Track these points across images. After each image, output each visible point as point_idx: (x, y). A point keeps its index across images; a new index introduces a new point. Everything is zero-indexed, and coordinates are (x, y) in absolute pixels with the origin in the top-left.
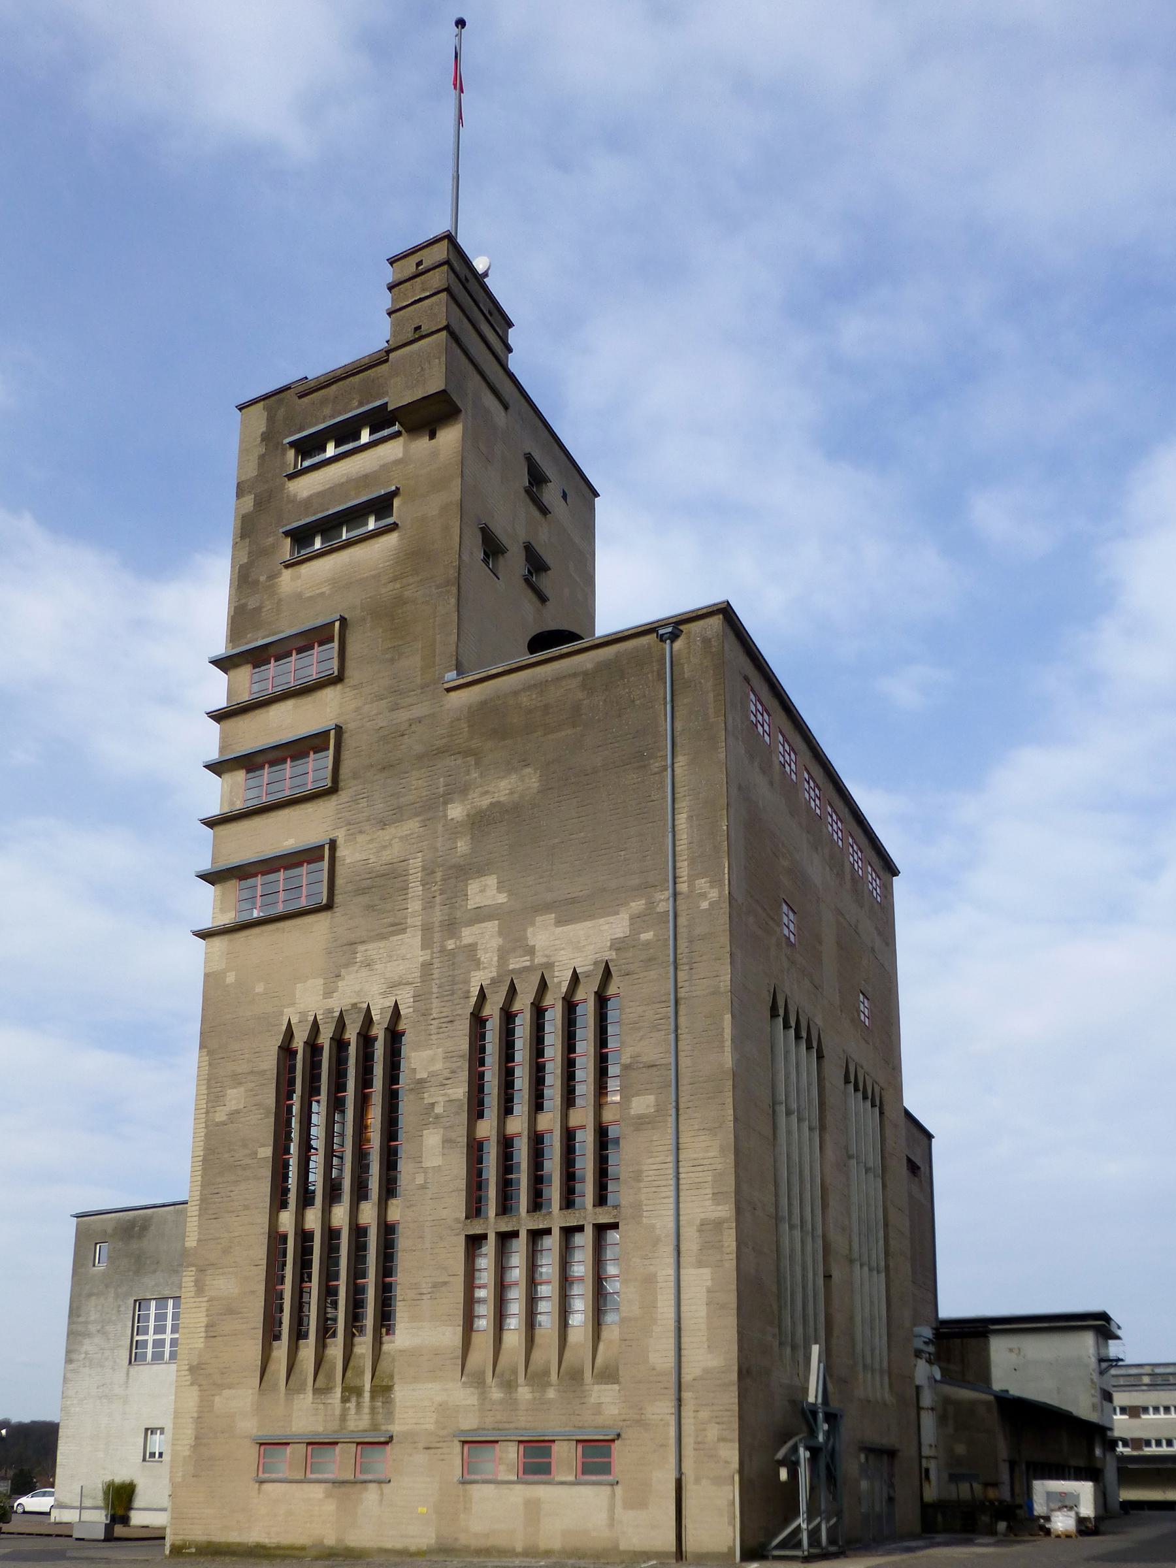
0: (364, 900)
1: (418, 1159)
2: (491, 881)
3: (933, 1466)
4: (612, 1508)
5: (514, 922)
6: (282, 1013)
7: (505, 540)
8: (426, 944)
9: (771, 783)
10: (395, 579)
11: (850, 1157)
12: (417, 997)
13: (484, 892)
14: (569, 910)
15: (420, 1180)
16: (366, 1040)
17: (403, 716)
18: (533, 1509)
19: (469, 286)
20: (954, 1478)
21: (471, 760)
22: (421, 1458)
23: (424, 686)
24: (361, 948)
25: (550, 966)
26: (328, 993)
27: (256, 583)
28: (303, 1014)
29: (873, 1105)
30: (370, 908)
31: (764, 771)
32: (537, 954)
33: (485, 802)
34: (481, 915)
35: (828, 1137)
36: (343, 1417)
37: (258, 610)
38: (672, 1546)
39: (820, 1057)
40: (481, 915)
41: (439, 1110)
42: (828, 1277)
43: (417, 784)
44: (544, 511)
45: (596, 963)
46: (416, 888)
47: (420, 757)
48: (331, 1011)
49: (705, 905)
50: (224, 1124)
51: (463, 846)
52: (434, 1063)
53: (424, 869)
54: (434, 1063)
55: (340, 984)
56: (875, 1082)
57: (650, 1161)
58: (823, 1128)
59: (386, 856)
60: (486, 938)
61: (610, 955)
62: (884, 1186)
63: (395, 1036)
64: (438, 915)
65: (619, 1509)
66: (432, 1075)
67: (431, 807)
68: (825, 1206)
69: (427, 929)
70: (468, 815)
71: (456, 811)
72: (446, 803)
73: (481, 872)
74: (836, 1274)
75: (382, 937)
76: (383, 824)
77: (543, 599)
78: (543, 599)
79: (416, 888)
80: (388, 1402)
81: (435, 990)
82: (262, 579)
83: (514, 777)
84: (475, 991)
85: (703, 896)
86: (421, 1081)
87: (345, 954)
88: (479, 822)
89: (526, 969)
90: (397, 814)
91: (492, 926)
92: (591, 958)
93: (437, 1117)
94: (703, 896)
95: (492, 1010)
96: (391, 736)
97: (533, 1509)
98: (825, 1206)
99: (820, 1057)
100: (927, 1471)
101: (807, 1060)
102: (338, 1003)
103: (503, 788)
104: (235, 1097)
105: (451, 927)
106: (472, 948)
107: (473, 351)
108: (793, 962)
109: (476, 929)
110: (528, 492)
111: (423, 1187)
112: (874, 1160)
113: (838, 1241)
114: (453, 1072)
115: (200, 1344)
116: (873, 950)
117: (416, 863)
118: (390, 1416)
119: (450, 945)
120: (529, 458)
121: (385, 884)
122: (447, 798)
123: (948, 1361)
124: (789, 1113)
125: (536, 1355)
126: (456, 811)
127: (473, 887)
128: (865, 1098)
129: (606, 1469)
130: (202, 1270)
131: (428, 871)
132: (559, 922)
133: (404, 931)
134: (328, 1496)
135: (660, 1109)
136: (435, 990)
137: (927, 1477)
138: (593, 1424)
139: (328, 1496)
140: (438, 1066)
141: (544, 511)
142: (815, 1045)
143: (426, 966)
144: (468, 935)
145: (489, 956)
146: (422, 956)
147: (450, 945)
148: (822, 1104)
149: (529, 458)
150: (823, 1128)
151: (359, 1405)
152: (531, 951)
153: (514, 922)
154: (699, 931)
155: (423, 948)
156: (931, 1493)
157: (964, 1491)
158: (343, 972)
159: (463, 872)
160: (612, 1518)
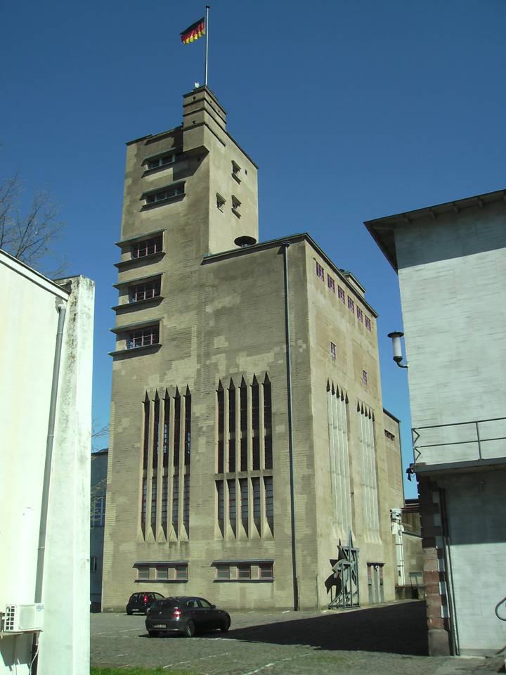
0: (175, 343)
1: (196, 449)
2: (222, 338)
3: (401, 569)
4: (272, 590)
5: (231, 354)
6: (143, 389)
7: (225, 197)
8: (199, 362)
9: (325, 296)
10: (185, 215)
11: (361, 441)
12: (195, 384)
13: (220, 342)
14: (253, 350)
15: (197, 458)
16: (178, 399)
17: (189, 270)
18: (243, 594)
19: (211, 104)
20: (411, 574)
21: (215, 289)
22: (199, 571)
23: (196, 258)
24: (174, 362)
25: (245, 372)
26: (161, 381)
27: (133, 213)
28: (151, 389)
29: (370, 418)
30: (177, 346)
31: (322, 293)
32: (240, 367)
33: (220, 306)
34: (219, 351)
35: (351, 435)
36: (169, 555)
37: (133, 224)
38: (292, 604)
39: (347, 402)
40: (219, 351)
41: (204, 429)
42: (353, 493)
43: (193, 298)
44: (239, 181)
45: (262, 372)
46: (194, 340)
47: (196, 286)
48: (162, 388)
49: (301, 350)
50: (121, 433)
51: (212, 323)
52: (205, 411)
53: (197, 331)
54: (205, 411)
55: (166, 377)
56: (370, 408)
57: (283, 451)
58: (349, 431)
59: (183, 326)
60: (221, 360)
61: (268, 369)
62: (376, 451)
63: (188, 397)
64: (202, 351)
65: (275, 591)
66: (202, 415)
67: (200, 308)
68: (351, 463)
69: (199, 356)
70: (214, 311)
71: (209, 309)
72: (205, 305)
73: (219, 334)
74: (355, 492)
75: (182, 358)
76: (181, 312)
77: (238, 216)
78: (238, 216)
79: (194, 340)
80: (187, 549)
81: (202, 380)
82: (135, 211)
83: (231, 297)
84: (217, 382)
85: (300, 347)
86: (198, 417)
87: (167, 365)
88: (218, 314)
89: (235, 373)
90: (187, 309)
91: (224, 355)
92: (260, 371)
93: (204, 432)
94: (300, 347)
95: (226, 386)
96: (183, 277)
97: (243, 594)
98: (351, 463)
99: (347, 402)
100: (400, 572)
101: (342, 404)
102: (165, 385)
103: (226, 301)
104: (126, 422)
105: (208, 355)
106: (216, 364)
107: (213, 129)
108: (335, 366)
109: (218, 356)
110: (233, 211)
111: (199, 461)
112: (370, 440)
113: (357, 479)
114: (210, 414)
115: (114, 524)
116: (368, 352)
117: (194, 329)
118: (188, 554)
119: (208, 362)
120: (233, 162)
121: (182, 338)
122: (206, 303)
123: (407, 523)
124: (335, 428)
125: (147, 536)
126: (209, 309)
127: (216, 340)
128: (366, 415)
129: (271, 574)
130: (113, 494)
131: (199, 333)
132: (248, 356)
133: (189, 356)
134: (165, 586)
135: (175, 624)
136: (202, 380)
137: (400, 575)
138: (264, 557)
139: (165, 586)
140: (204, 412)
141: (239, 181)
142: (345, 398)
143: (199, 370)
144: (214, 359)
145: (222, 367)
146: (198, 366)
147: (208, 362)
148: (348, 421)
149: (233, 162)
150: (349, 431)
151: (176, 549)
152: (238, 366)
153: (231, 354)
154: (299, 361)
155: (198, 363)
156: (402, 582)
157: (413, 582)
158: (167, 372)
159: (211, 334)
160: (273, 594)
